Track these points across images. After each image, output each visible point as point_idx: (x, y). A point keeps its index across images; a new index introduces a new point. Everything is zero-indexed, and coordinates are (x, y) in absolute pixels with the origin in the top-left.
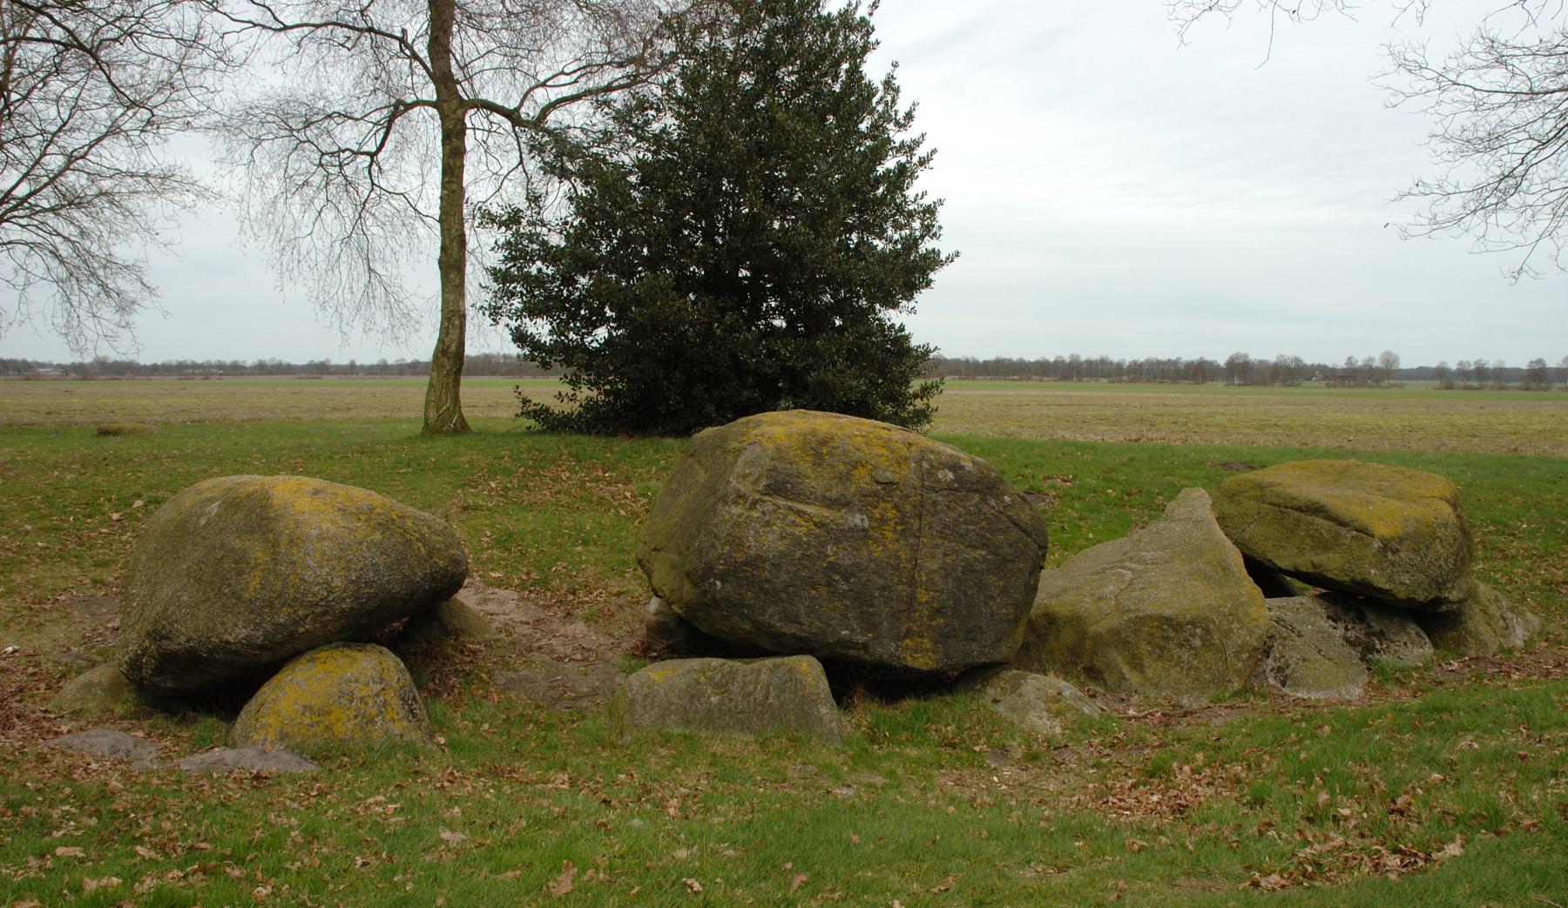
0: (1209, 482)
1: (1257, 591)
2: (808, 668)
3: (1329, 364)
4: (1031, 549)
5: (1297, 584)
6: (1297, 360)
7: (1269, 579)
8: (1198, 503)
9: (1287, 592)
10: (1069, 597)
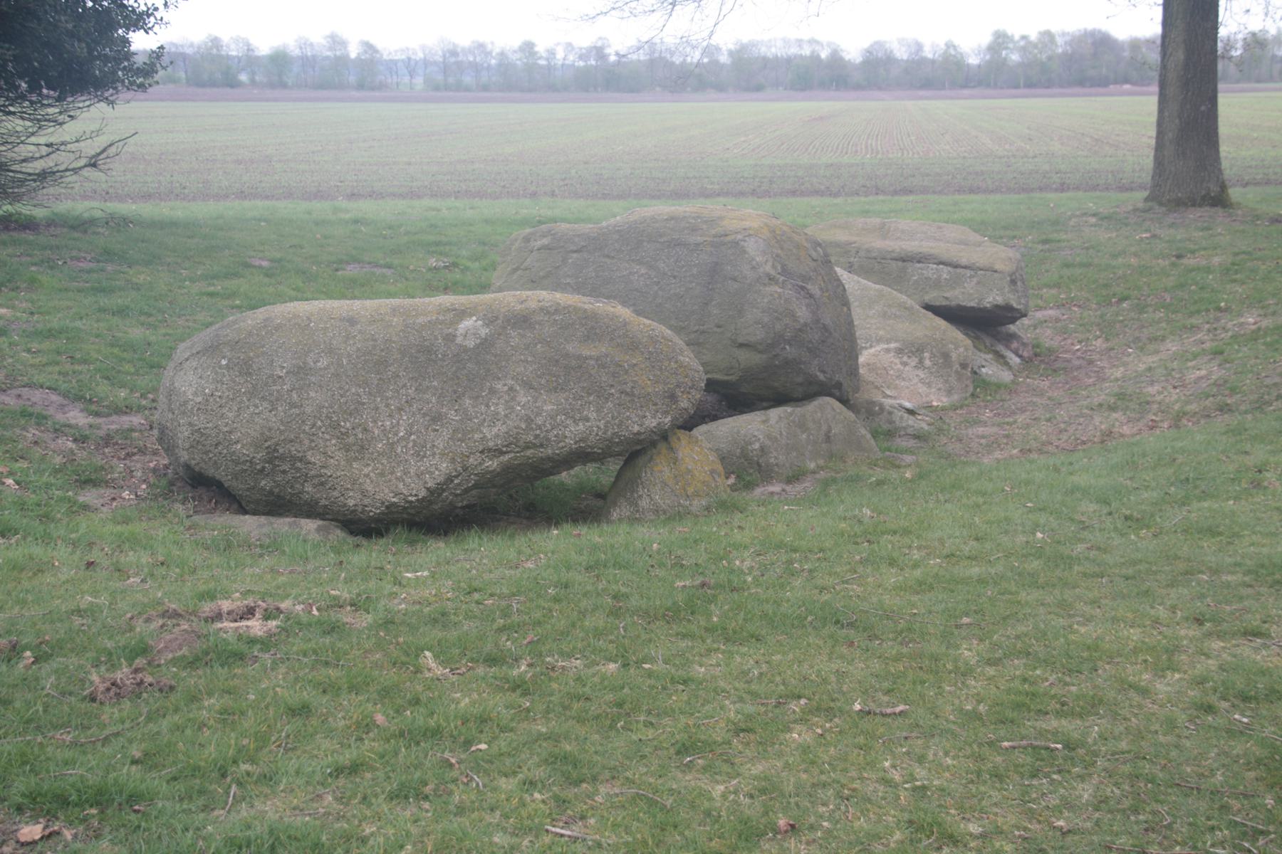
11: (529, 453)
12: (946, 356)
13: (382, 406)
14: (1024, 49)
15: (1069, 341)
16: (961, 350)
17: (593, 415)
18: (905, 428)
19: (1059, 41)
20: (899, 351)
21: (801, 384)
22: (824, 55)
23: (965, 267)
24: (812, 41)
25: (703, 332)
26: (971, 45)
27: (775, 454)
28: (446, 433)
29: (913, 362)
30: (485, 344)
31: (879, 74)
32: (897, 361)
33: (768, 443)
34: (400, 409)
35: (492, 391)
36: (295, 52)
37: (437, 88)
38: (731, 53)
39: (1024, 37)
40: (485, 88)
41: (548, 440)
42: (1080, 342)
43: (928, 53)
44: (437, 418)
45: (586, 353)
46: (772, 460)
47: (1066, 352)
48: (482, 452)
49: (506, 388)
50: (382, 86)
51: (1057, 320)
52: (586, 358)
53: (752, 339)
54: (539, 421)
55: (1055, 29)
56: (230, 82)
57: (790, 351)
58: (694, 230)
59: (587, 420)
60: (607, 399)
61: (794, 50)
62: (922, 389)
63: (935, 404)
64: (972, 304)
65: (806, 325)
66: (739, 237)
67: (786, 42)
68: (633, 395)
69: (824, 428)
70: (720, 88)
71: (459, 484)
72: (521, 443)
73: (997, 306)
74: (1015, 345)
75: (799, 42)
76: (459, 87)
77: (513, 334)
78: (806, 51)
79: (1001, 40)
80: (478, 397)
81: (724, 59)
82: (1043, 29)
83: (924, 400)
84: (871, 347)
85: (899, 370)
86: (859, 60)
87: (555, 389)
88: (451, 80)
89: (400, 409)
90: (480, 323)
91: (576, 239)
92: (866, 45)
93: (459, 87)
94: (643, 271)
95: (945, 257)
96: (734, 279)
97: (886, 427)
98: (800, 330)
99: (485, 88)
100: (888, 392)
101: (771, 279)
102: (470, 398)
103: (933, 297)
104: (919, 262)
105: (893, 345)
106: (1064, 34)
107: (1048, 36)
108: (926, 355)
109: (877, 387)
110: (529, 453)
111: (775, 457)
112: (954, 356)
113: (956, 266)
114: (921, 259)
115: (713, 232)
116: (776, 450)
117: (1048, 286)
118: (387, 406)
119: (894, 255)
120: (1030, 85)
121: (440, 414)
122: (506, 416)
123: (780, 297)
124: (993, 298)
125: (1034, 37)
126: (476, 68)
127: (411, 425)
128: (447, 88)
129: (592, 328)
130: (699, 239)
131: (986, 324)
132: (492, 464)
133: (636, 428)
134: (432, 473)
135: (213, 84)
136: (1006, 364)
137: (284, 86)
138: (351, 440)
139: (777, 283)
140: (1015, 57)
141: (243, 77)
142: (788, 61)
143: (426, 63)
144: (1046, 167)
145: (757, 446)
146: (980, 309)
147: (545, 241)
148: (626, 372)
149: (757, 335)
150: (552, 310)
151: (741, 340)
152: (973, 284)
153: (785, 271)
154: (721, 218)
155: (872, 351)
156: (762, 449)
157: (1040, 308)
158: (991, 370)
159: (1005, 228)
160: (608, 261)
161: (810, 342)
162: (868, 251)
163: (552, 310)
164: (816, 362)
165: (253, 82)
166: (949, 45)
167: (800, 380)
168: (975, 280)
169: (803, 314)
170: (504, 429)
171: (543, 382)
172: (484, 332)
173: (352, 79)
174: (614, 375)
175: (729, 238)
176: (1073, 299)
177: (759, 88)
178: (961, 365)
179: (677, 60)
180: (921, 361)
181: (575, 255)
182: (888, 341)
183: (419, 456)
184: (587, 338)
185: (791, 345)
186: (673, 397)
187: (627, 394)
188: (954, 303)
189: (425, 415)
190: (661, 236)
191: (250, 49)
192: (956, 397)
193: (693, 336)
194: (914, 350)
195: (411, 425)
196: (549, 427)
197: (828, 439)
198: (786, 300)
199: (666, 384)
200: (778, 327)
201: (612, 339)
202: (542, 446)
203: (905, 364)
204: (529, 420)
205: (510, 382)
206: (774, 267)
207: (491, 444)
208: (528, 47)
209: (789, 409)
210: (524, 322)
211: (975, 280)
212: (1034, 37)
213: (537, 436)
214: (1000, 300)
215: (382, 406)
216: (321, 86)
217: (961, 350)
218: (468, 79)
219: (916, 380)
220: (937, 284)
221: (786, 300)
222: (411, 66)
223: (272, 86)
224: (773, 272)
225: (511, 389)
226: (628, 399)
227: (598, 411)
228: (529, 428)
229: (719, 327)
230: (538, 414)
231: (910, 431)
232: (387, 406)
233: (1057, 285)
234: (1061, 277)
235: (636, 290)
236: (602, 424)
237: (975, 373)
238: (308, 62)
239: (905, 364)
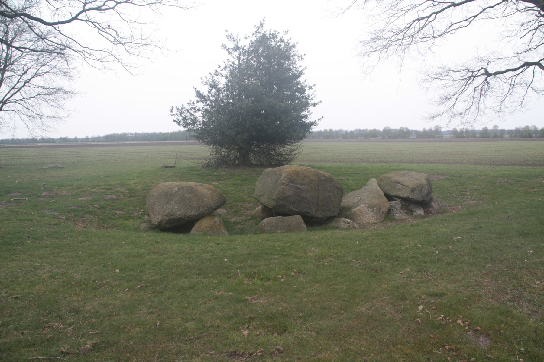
0: (377, 177)
1: (387, 200)
2: (299, 218)
3: (418, 129)
4: (340, 192)
5: (396, 199)
6: (407, 129)
7: (390, 198)
8: (373, 183)
9: (394, 200)
10: (347, 203)
20: (368, 207)
29: (371, 210)
57: (281, 202)
62: (371, 218)
69: (290, 223)
135: (526, 137)
141: (534, 135)
165: (536, 136)
186: (199, 208)
191: (535, 127)
203: (369, 210)
239: (369, 210)
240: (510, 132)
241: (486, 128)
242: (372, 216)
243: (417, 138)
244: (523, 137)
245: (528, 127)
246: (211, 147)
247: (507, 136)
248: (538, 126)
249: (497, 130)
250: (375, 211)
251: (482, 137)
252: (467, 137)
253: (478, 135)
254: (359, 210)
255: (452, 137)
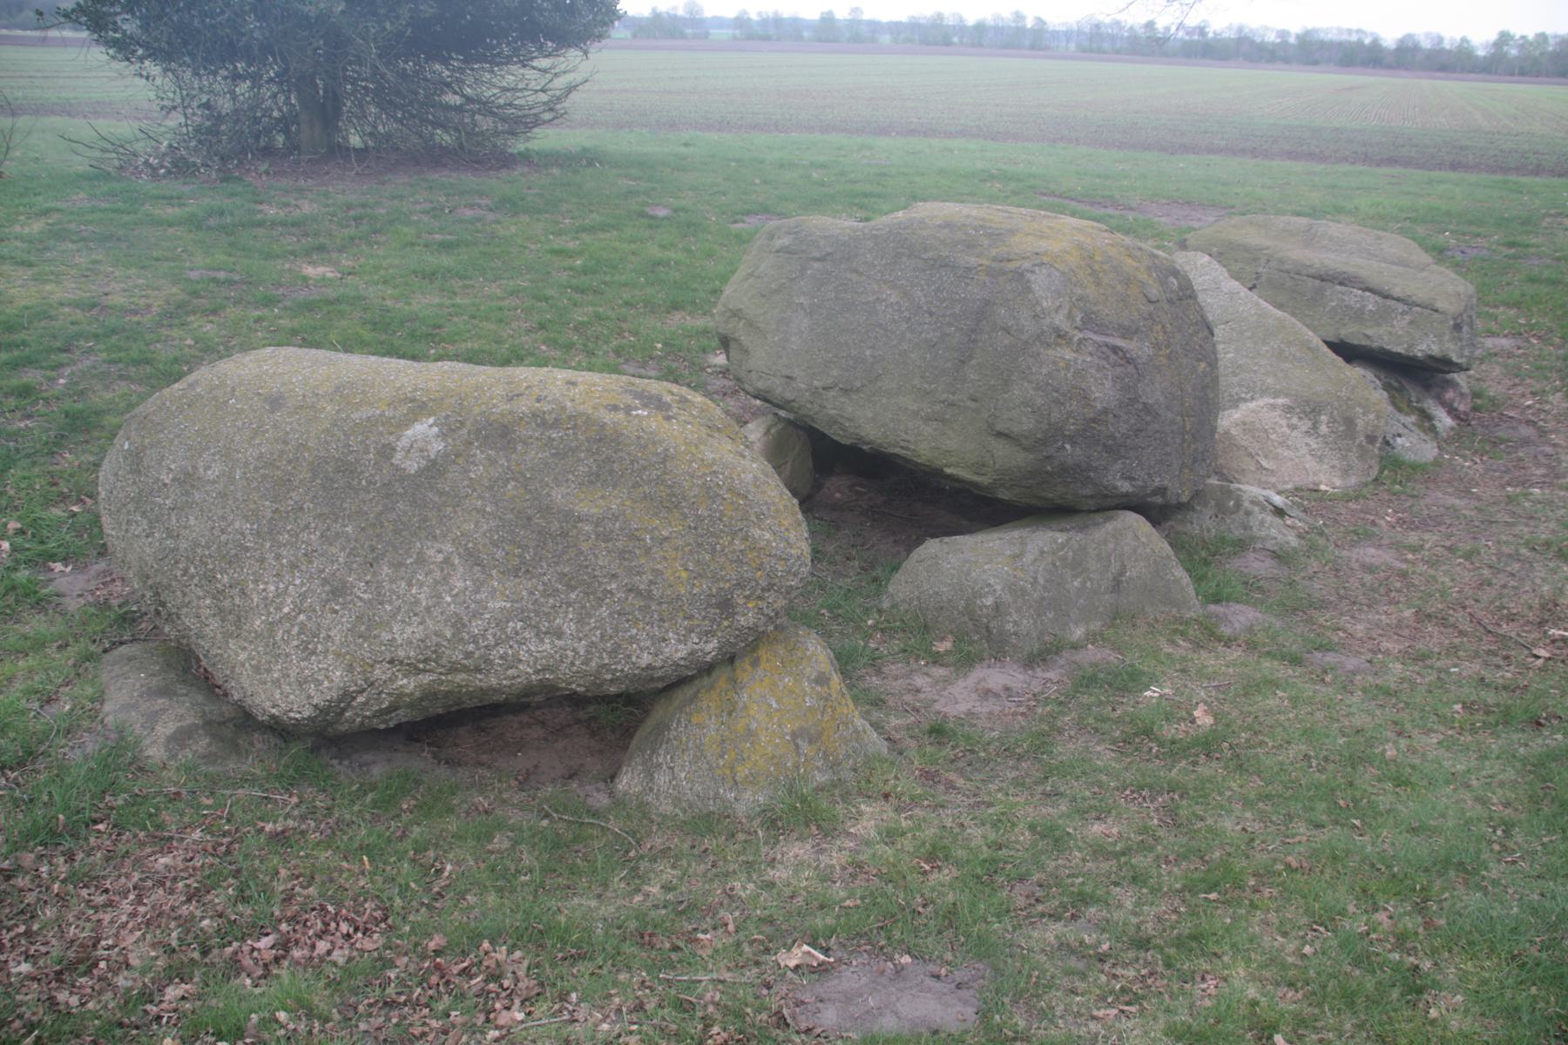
11: (460, 678)
12: (1350, 422)
13: (270, 556)
14: (1522, 46)
15: (1520, 389)
16: (1372, 416)
17: (569, 628)
18: (1264, 539)
19: (1551, 41)
20: (1288, 410)
21: (1092, 497)
22: (1367, 41)
23: (1398, 300)
24: (1359, 31)
25: (952, 405)
26: (1481, 38)
27: (1015, 617)
28: (347, 619)
29: (1305, 425)
30: (434, 469)
31: (1408, 58)
32: (1284, 422)
33: (1007, 598)
34: (294, 566)
35: (421, 560)
36: (990, 22)
37: (1084, 51)
38: (1298, 36)
39: (1523, 37)
40: (1118, 52)
41: (488, 661)
42: (1534, 394)
43: (1447, 45)
44: (339, 591)
45: (582, 508)
46: (1009, 627)
47: (1514, 406)
48: (391, 662)
49: (440, 557)
50: (1047, 48)
51: (1510, 355)
52: (580, 519)
53: (1016, 429)
54: (476, 627)
55: (1549, 32)
56: (947, 42)
57: (1071, 453)
58: (970, 245)
59: (559, 634)
60: (600, 601)
61: (1345, 37)
62: (1311, 464)
63: (1323, 487)
64: (1399, 349)
65: (1106, 411)
66: (1027, 265)
67: (1340, 30)
68: (650, 596)
69: (1115, 568)
70: (1287, 61)
71: (365, 704)
72: (444, 661)
73: (1431, 357)
74: (1450, 395)
75: (1350, 31)
76: (1100, 51)
77: (480, 456)
78: (1354, 38)
79: (1504, 38)
80: (400, 564)
81: (1292, 40)
82: (1539, 31)
83: (1311, 478)
84: (1252, 399)
85: (1284, 435)
86: (1393, 46)
87: (516, 572)
88: (1094, 46)
89: (294, 566)
90: (436, 429)
91: (822, 243)
92: (1399, 35)
93: (1100, 51)
94: (893, 299)
95: (1374, 282)
96: (1007, 330)
97: (1238, 533)
98: (1094, 420)
99: (1118, 52)
100: (1264, 463)
101: (1060, 335)
102: (391, 565)
103: (1352, 333)
104: (1341, 284)
105: (1280, 401)
106: (1556, 36)
107: (1542, 37)
108: (1324, 418)
109: (1250, 455)
110: (460, 678)
111: (1019, 622)
112: (1360, 424)
113: (1386, 297)
114: (1344, 280)
115: (994, 252)
116: (1018, 610)
117: (1509, 305)
118: (278, 557)
119: (1312, 271)
120: (1523, 73)
121: (344, 583)
122: (428, 609)
123: (1068, 367)
124: (1426, 346)
125: (1531, 37)
126: (1113, 38)
127: (303, 596)
128: (1091, 51)
129: (609, 459)
130: (973, 261)
131: (1411, 375)
132: (408, 684)
133: (646, 659)
134: (320, 683)
135: (936, 44)
136: (1433, 429)
137: (981, 45)
138: (227, 603)
139: (1069, 342)
140: (1514, 52)
141: (955, 40)
142: (1340, 44)
143: (1080, 32)
144: (1526, 147)
145: (989, 601)
146: (1408, 358)
147: (786, 241)
148: (648, 551)
149: (1025, 424)
150: (550, 418)
151: (999, 427)
152: (1404, 323)
153: (1090, 322)
154: (1012, 232)
155: (1252, 405)
156: (997, 607)
157: (1491, 334)
158: (1414, 446)
159: (1470, 223)
160: (854, 277)
161: (1112, 437)
162: (1281, 261)
163: (550, 418)
164: (1119, 466)
165: (961, 43)
166: (1464, 40)
167: (1088, 491)
168: (1408, 318)
169: (1104, 393)
170: (420, 632)
171: (499, 554)
172: (438, 446)
173: (1027, 43)
174: (622, 554)
175: (1011, 266)
176: (1532, 327)
177: (1316, 63)
178: (1367, 437)
179: (1258, 40)
180: (1315, 426)
181: (817, 265)
182: (1276, 395)
183: (307, 651)
184: (594, 478)
185: (1073, 444)
186: (726, 606)
187: (639, 593)
188: (1375, 345)
189: (325, 582)
190: (926, 250)
191: (961, 20)
192: (1353, 480)
193: (938, 407)
194: (1309, 409)
195: (303, 596)
196: (491, 640)
197: (1117, 585)
198: (1077, 373)
199: (715, 579)
200: (1056, 416)
201: (636, 485)
202: (478, 670)
203: (1293, 427)
204: (458, 624)
205: (448, 547)
206: (1070, 316)
207: (401, 653)
208: (1150, 25)
209: (1061, 538)
210: (503, 436)
211: (1408, 318)
212: (1531, 37)
213: (468, 655)
214: (1435, 350)
215: (270, 556)
216: (1005, 47)
217: (1372, 416)
218: (1106, 46)
219: (1304, 450)
220: (1358, 316)
221: (1077, 373)
222: (1068, 35)
223: (973, 45)
224: (1065, 326)
225: (447, 561)
226: (639, 603)
227: (580, 621)
228: (457, 639)
229: (975, 400)
230: (476, 615)
231: (1270, 545)
232: (278, 557)
233: (1517, 305)
234: (1523, 295)
235: (880, 325)
236: (581, 647)
237: (1387, 443)
238: (998, 30)
239: (1293, 427)
240: (895, 28)
241: (830, 12)
242: (1312, 452)
243: (635, 36)
244: (928, 44)
245: (940, 16)
246: (111, 52)
247: (886, 39)
248: (965, 16)
249: (860, 22)
250: (1324, 429)
251: (820, 40)
252: (779, 39)
253: (806, 34)
254: (1247, 427)
255: (735, 38)
